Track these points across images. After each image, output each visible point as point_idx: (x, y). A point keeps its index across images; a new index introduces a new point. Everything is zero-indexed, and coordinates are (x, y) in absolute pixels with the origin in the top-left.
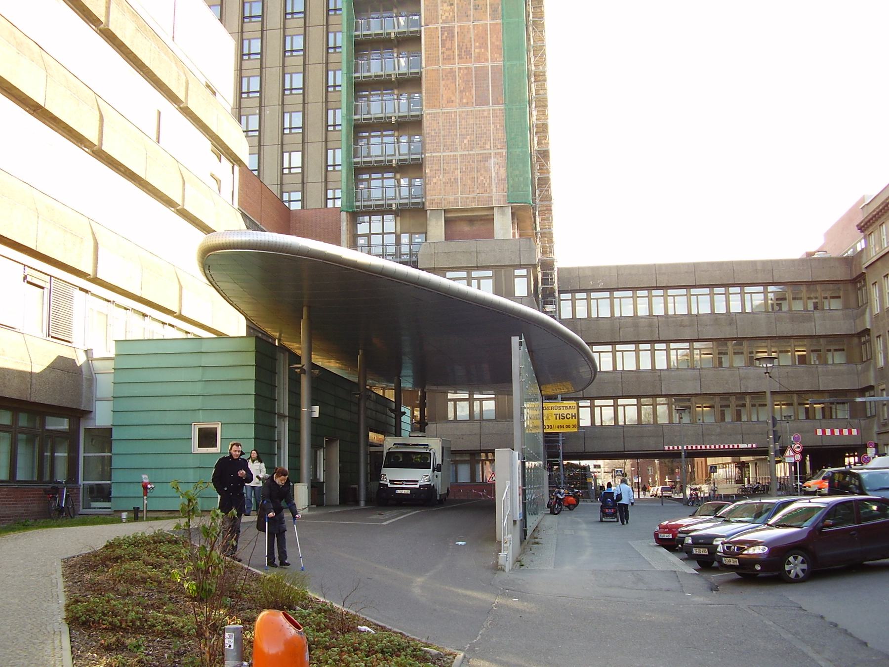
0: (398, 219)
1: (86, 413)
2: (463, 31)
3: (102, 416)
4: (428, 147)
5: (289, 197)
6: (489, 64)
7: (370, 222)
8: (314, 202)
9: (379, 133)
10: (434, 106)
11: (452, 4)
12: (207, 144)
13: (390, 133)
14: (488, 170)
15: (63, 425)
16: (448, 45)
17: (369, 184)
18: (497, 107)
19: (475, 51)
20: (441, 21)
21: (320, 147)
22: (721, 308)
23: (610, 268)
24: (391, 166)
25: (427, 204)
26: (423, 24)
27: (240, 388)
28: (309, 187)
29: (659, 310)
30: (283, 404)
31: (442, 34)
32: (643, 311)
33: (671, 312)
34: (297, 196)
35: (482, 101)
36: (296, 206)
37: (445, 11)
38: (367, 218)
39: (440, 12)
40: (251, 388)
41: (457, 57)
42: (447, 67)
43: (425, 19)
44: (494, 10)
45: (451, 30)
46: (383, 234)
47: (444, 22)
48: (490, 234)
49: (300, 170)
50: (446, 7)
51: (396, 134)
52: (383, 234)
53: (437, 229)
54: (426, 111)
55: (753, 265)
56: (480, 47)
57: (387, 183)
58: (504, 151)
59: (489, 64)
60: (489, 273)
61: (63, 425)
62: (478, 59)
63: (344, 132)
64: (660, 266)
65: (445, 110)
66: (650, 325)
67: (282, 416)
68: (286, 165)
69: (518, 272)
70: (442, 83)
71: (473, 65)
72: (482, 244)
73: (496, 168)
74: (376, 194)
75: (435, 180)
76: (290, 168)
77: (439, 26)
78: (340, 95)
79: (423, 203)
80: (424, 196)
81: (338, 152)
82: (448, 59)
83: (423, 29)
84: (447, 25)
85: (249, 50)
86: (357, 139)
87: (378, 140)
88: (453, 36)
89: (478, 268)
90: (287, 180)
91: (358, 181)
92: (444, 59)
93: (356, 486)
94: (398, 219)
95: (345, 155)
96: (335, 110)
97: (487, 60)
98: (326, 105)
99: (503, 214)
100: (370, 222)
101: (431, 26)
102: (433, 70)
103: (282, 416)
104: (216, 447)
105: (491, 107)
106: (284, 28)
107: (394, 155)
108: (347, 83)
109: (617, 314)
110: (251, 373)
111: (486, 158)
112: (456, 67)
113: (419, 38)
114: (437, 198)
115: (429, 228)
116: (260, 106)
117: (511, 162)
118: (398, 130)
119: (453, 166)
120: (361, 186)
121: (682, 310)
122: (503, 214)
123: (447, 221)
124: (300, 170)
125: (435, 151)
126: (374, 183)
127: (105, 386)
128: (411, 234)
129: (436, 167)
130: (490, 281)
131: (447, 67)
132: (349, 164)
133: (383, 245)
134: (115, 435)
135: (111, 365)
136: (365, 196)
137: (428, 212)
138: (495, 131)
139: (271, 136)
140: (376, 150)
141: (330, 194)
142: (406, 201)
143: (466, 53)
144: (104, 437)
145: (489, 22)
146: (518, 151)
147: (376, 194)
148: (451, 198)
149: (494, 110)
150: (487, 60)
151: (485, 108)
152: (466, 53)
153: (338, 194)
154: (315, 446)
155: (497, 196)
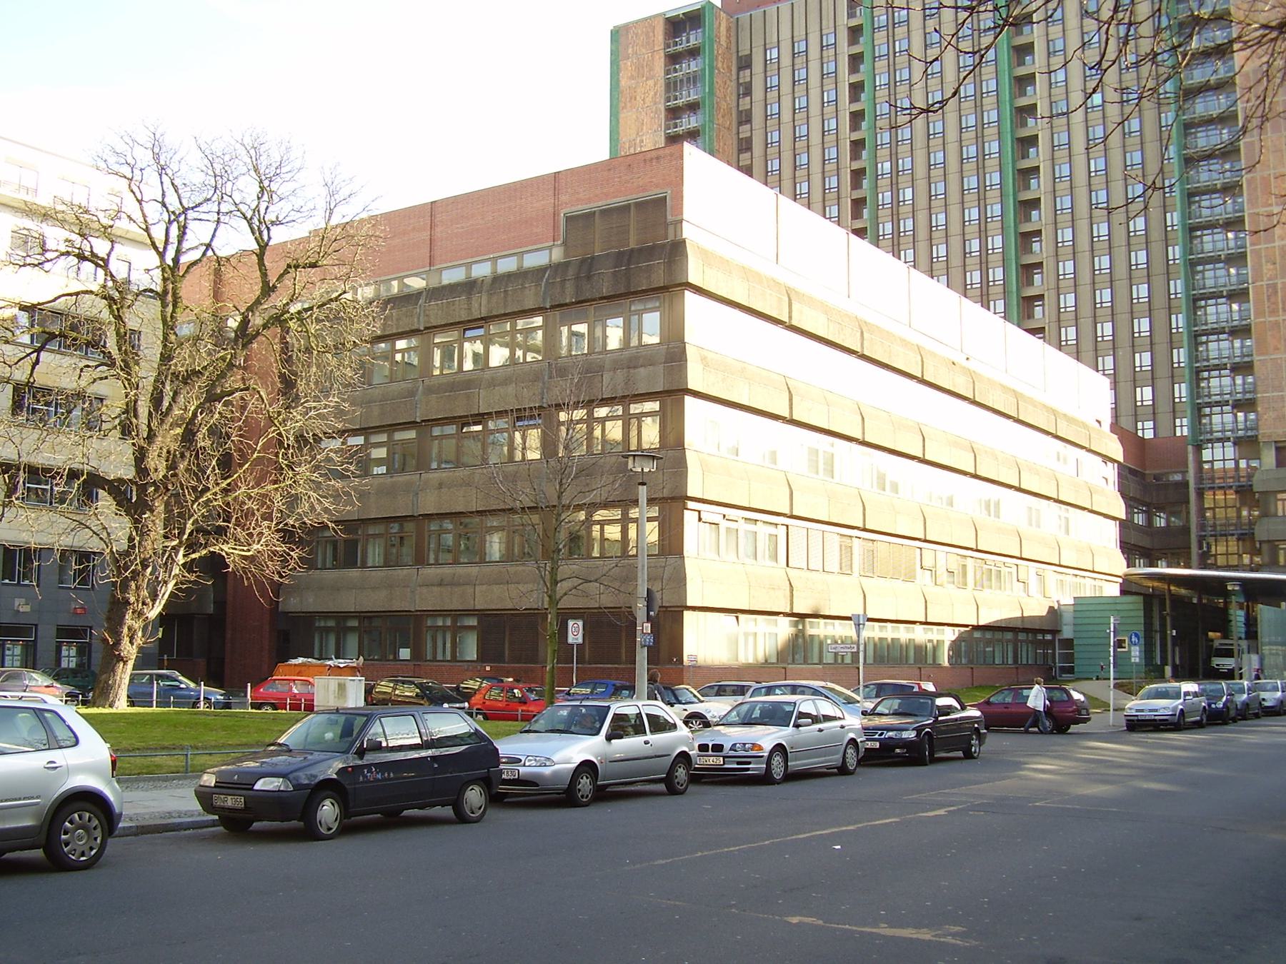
0: (1237, 447)
5: (1143, 426)
7: (1212, 448)
8: (1164, 433)
9: (1204, 129)
10: (1262, 354)
11: (1275, 264)
13: (1213, 127)
17: (1204, 274)
20: (1265, 279)
24: (1219, 224)
25: (1260, 437)
26: (1250, 282)
28: (1159, 417)
30: (1157, 625)
31: (1268, 291)
34: (1150, 424)
36: (1149, 435)
37: (1269, 270)
38: (1210, 445)
39: (1265, 271)
41: (1281, 310)
43: (1252, 278)
45: (1274, 286)
47: (1269, 279)
51: (1220, 162)
52: (1224, 460)
57: (1217, 237)
63: (1176, 164)
65: (1273, 357)
67: (1156, 631)
68: (1135, 296)
70: (1269, 333)
74: (1208, 247)
75: (1265, 417)
76: (1138, 298)
78: (1182, 337)
79: (1257, 436)
80: (1256, 429)
81: (1183, 385)
82: (1274, 312)
83: (1250, 286)
84: (1271, 282)
85: (1100, 266)
86: (1186, 135)
87: (1204, 134)
88: (1277, 292)
90: (1136, 308)
91: (1192, 238)
92: (1270, 312)
94: (1237, 447)
95: (1187, 352)
98: (1168, 277)
100: (1212, 448)
102: (1261, 322)
103: (1156, 631)
106: (1131, 278)
107: (1223, 250)
108: (1188, 337)
113: (1244, 220)
115: (1262, 457)
118: (1221, 158)
123: (1277, 449)
124: (1151, 403)
126: (1205, 238)
128: (1248, 459)
129: (1266, 406)
132: (1184, 226)
133: (1215, 277)
136: (1198, 214)
137: (1261, 444)
139: (1124, 374)
140: (1204, 176)
141: (1178, 422)
142: (1233, 251)
147: (1208, 247)
153: (1185, 421)
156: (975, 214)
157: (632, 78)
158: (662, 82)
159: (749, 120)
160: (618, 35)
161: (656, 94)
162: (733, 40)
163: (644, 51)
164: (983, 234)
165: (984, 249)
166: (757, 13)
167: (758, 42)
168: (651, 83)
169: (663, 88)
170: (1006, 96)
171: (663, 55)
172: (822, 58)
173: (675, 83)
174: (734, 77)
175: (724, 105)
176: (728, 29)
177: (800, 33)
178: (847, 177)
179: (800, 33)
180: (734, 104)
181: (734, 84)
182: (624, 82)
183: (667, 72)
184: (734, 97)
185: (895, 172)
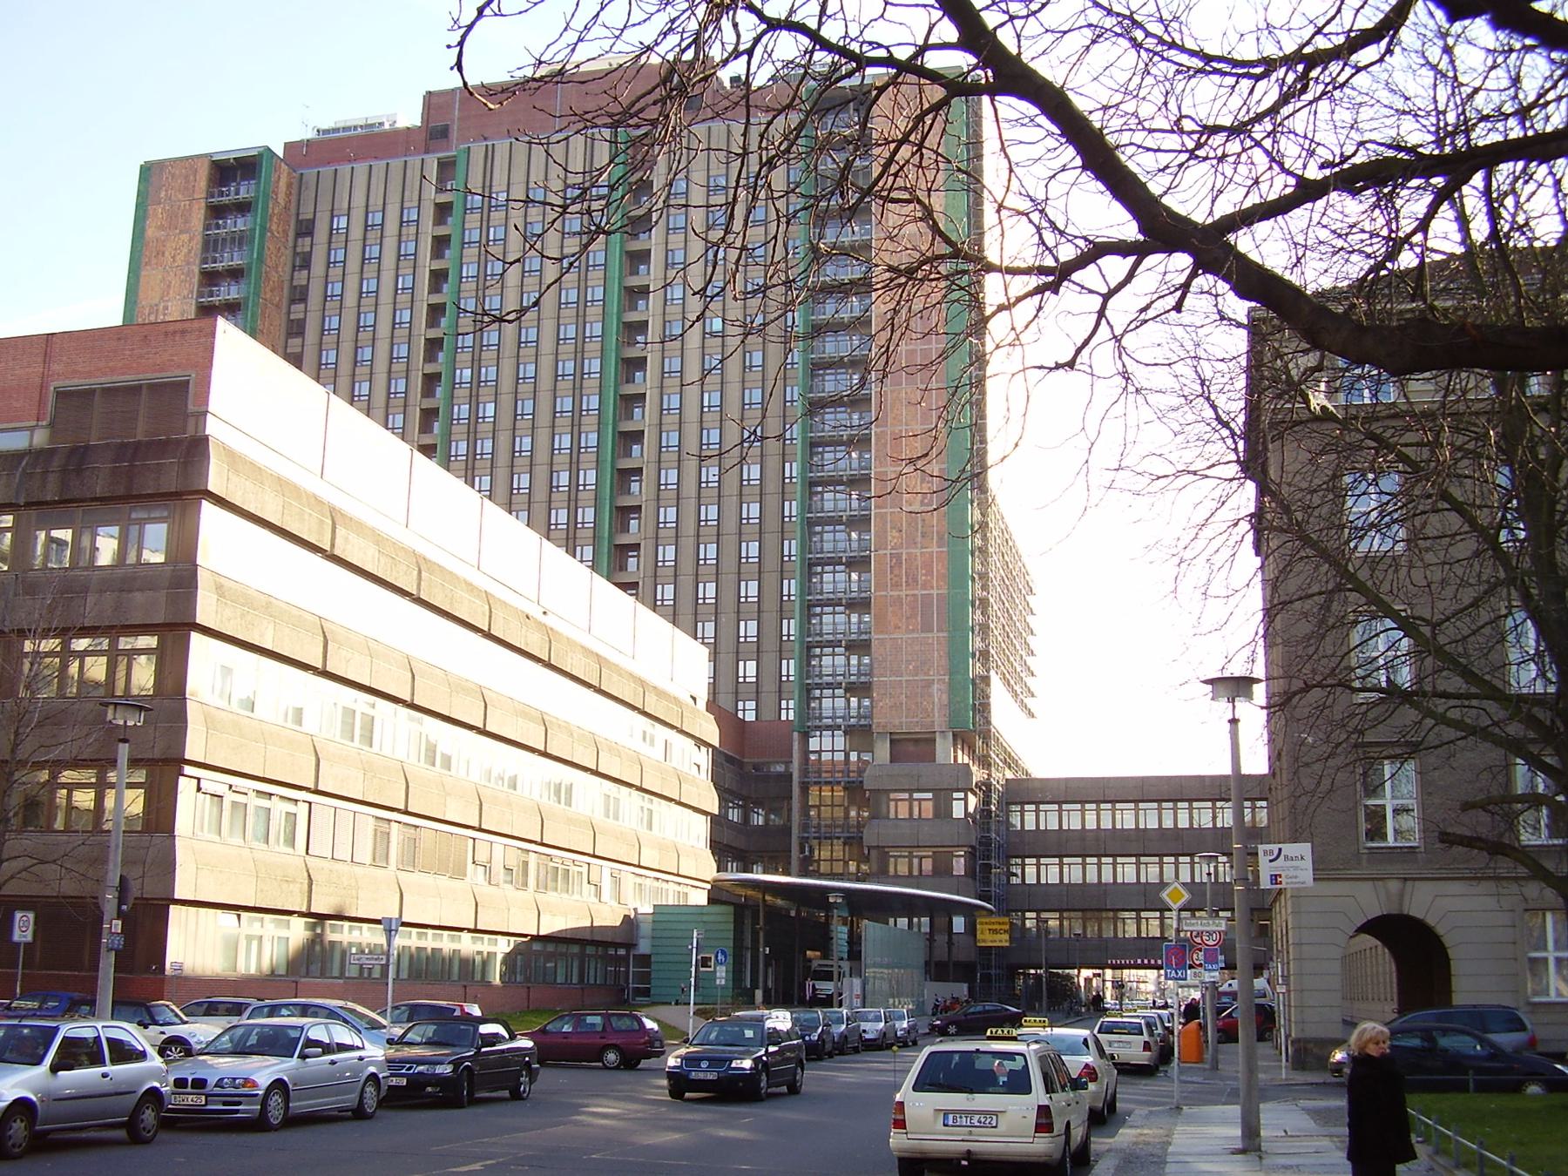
1: (634, 946)
2: (910, 558)
3: (644, 947)
4: (875, 671)
6: (935, 592)
8: (768, 715)
10: (882, 632)
12: (691, 742)
14: (931, 695)
15: (622, 952)
16: (896, 572)
18: (941, 634)
19: (921, 579)
21: (777, 498)
22: (1168, 823)
23: (1058, 780)
27: (722, 927)
29: (1106, 824)
30: (748, 942)
32: (1091, 824)
33: (1118, 826)
34: (751, 705)
35: (927, 628)
36: (750, 717)
38: (818, 733)
40: (731, 935)
42: (895, 593)
44: (941, 538)
45: (899, 556)
46: (833, 751)
48: (931, 757)
49: (754, 680)
50: (895, 534)
53: (883, 751)
54: (874, 636)
55: (1201, 779)
56: (926, 575)
58: (947, 678)
59: (935, 592)
60: (930, 795)
61: (622, 952)
62: (924, 587)
64: (1109, 779)
66: (1097, 839)
69: (955, 795)
70: (890, 609)
71: (920, 592)
72: (923, 767)
73: (939, 694)
77: (888, 552)
80: (871, 717)
81: (792, 662)
82: (896, 586)
89: (919, 791)
93: (957, 1057)
96: (789, 619)
97: (932, 588)
99: (945, 738)
101: (880, 552)
104: (1415, 1158)
105: (935, 634)
109: (1065, 827)
110: (731, 926)
111: (929, 684)
112: (903, 594)
114: (883, 721)
116: (716, 613)
117: (954, 689)
119: (899, 691)
120: (813, 705)
121: (1129, 824)
122: (945, 738)
123: (892, 741)
124: (754, 680)
125: (882, 676)
127: (646, 929)
130: (930, 804)
131: (895, 593)
134: (653, 959)
135: (650, 917)
138: (938, 657)
139: (727, 645)
143: (912, 581)
144: (645, 960)
145: (935, 549)
146: (959, 677)
148: (897, 722)
149: (936, 636)
150: (932, 588)
151: (930, 635)
152: (912, 581)
154: (767, 966)
155: (939, 721)
156: (564, 479)
157: (162, 227)
158: (199, 239)
159: (310, 233)
160: (150, 173)
161: (190, 251)
162: (294, 199)
163: (180, 196)
164: (574, 467)
165: (574, 484)
166: (327, 171)
167: (324, 206)
168: (185, 237)
169: (199, 246)
170: (614, 308)
171: (203, 205)
172: (400, 235)
173: (216, 241)
174: (291, 244)
175: (274, 277)
176: (289, 186)
177: (376, 200)
178: (418, 382)
179: (376, 200)
180: (287, 277)
181: (289, 252)
182: (151, 232)
183: (207, 227)
184: (288, 269)
185: (477, 381)
